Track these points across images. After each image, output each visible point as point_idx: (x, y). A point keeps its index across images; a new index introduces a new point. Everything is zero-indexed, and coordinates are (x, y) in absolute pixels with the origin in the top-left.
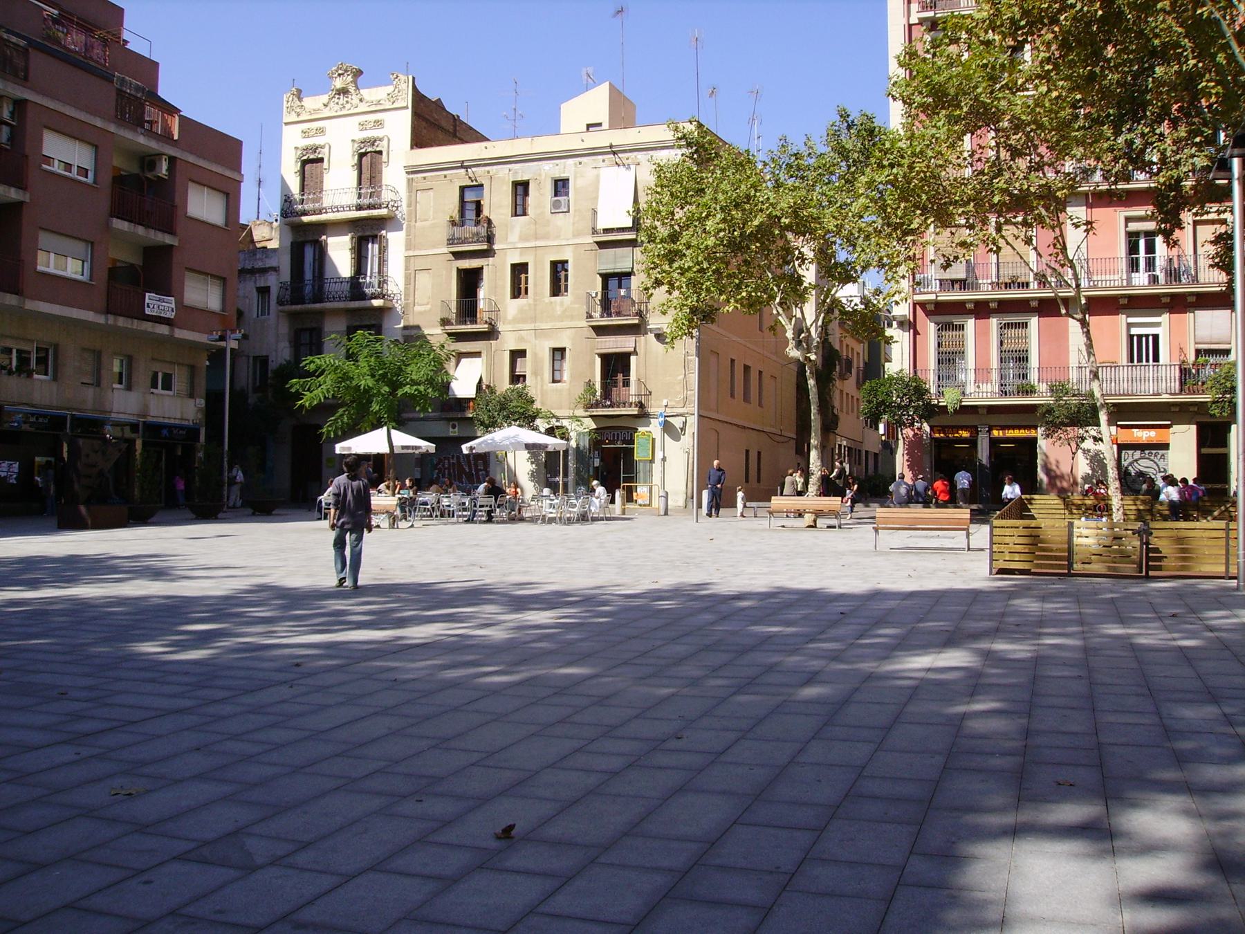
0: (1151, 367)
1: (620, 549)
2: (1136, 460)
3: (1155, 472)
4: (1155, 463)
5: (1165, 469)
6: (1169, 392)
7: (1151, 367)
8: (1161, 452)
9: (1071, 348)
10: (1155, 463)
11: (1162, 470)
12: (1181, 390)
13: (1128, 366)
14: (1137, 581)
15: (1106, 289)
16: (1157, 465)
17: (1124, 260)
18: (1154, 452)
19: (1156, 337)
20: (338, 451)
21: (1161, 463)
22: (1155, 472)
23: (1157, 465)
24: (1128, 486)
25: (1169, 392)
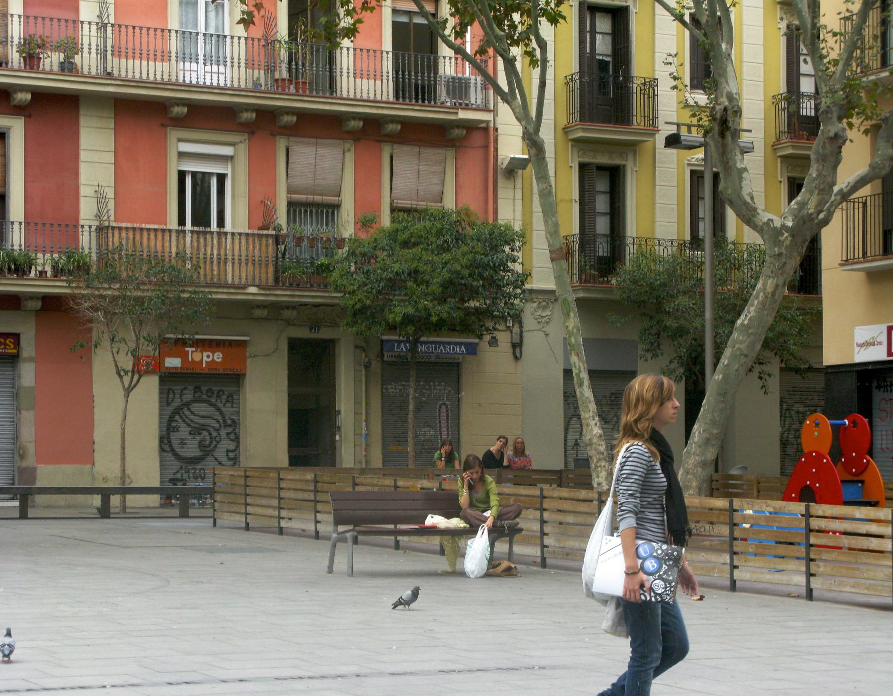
0: (188, 236)
1: (561, 523)
2: (187, 404)
3: (217, 426)
4: (219, 409)
5: (233, 421)
6: (257, 282)
7: (188, 236)
8: (228, 389)
9: (84, 191)
10: (219, 409)
11: (229, 422)
12: (276, 280)
13: (247, 235)
14: (777, 588)
15: (127, 82)
16: (221, 413)
17: (390, 55)
18: (216, 389)
19: (221, 178)
20: (167, 365)
21: (227, 409)
22: (217, 426)
23: (221, 413)
24: (173, 451)
25: (257, 282)
